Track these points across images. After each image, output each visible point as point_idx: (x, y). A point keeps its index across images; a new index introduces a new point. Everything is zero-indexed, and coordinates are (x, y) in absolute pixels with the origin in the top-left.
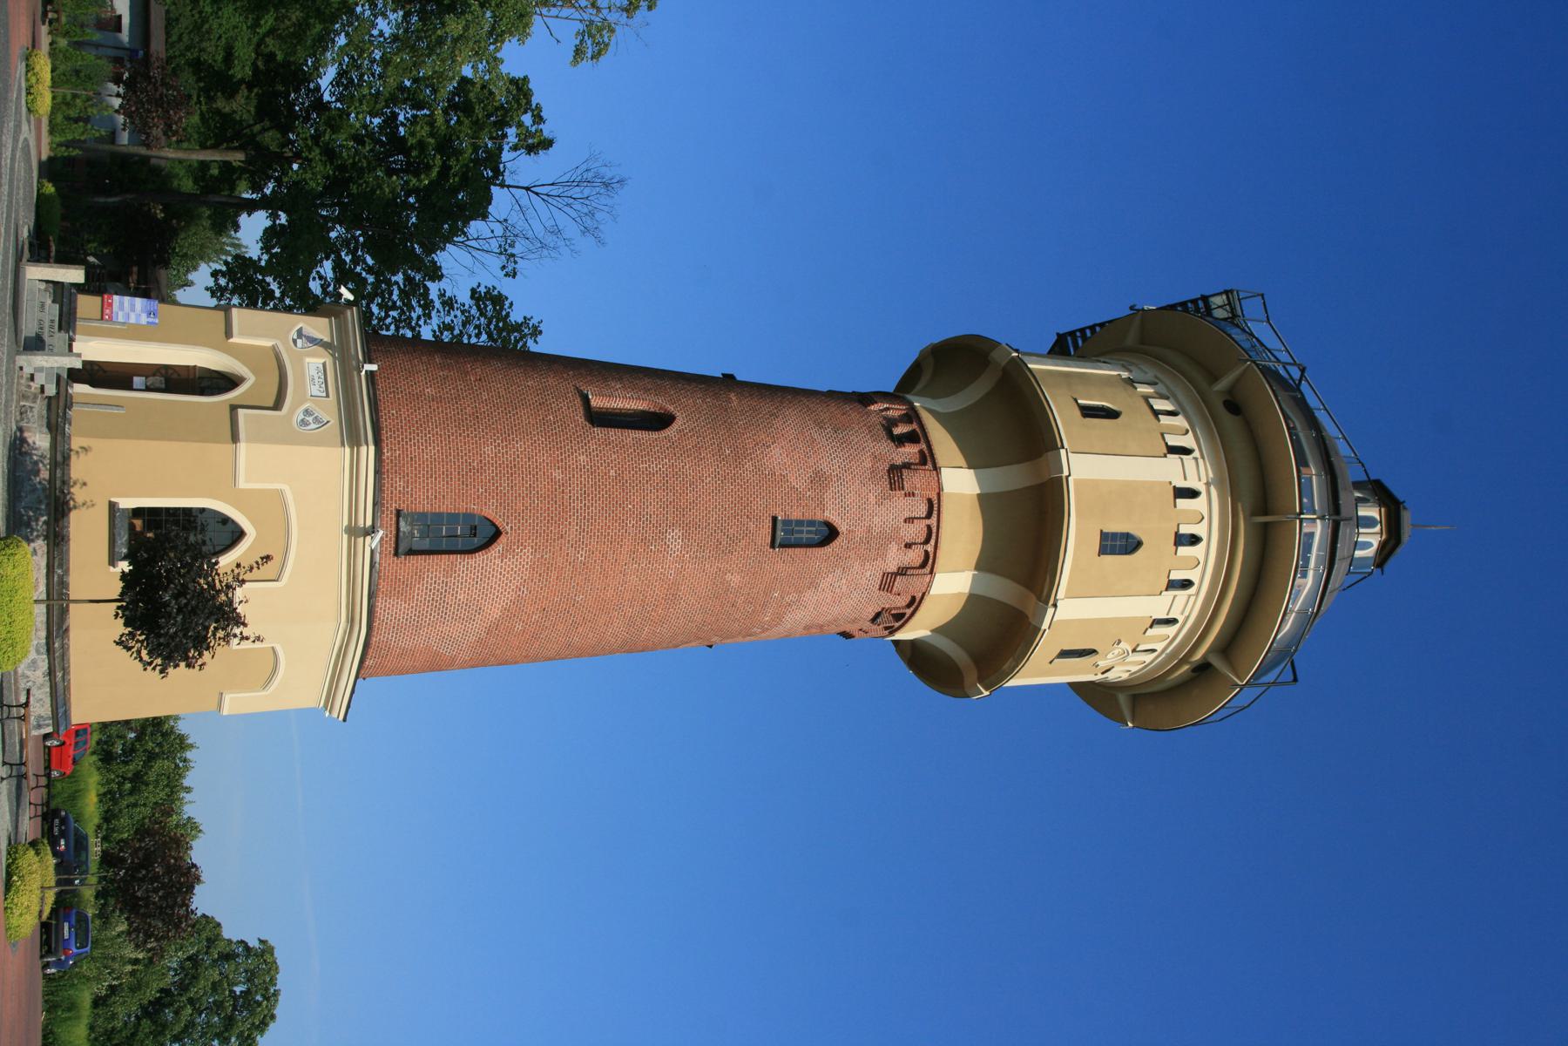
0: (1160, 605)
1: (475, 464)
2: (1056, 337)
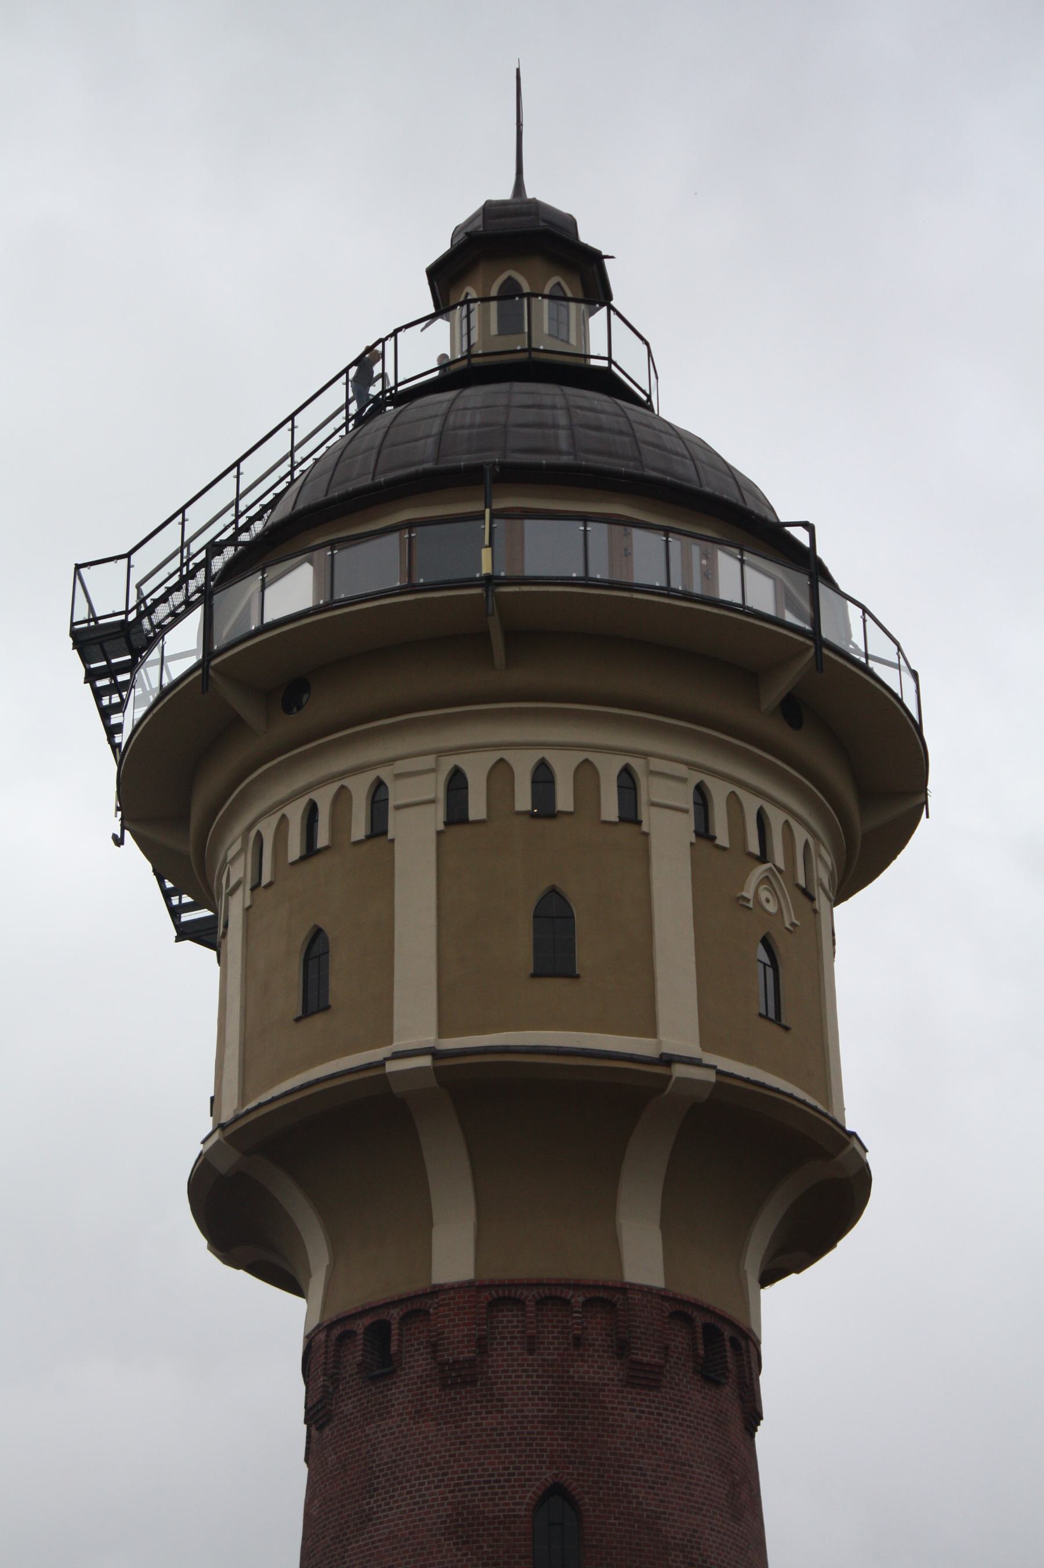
2: (188, 943)
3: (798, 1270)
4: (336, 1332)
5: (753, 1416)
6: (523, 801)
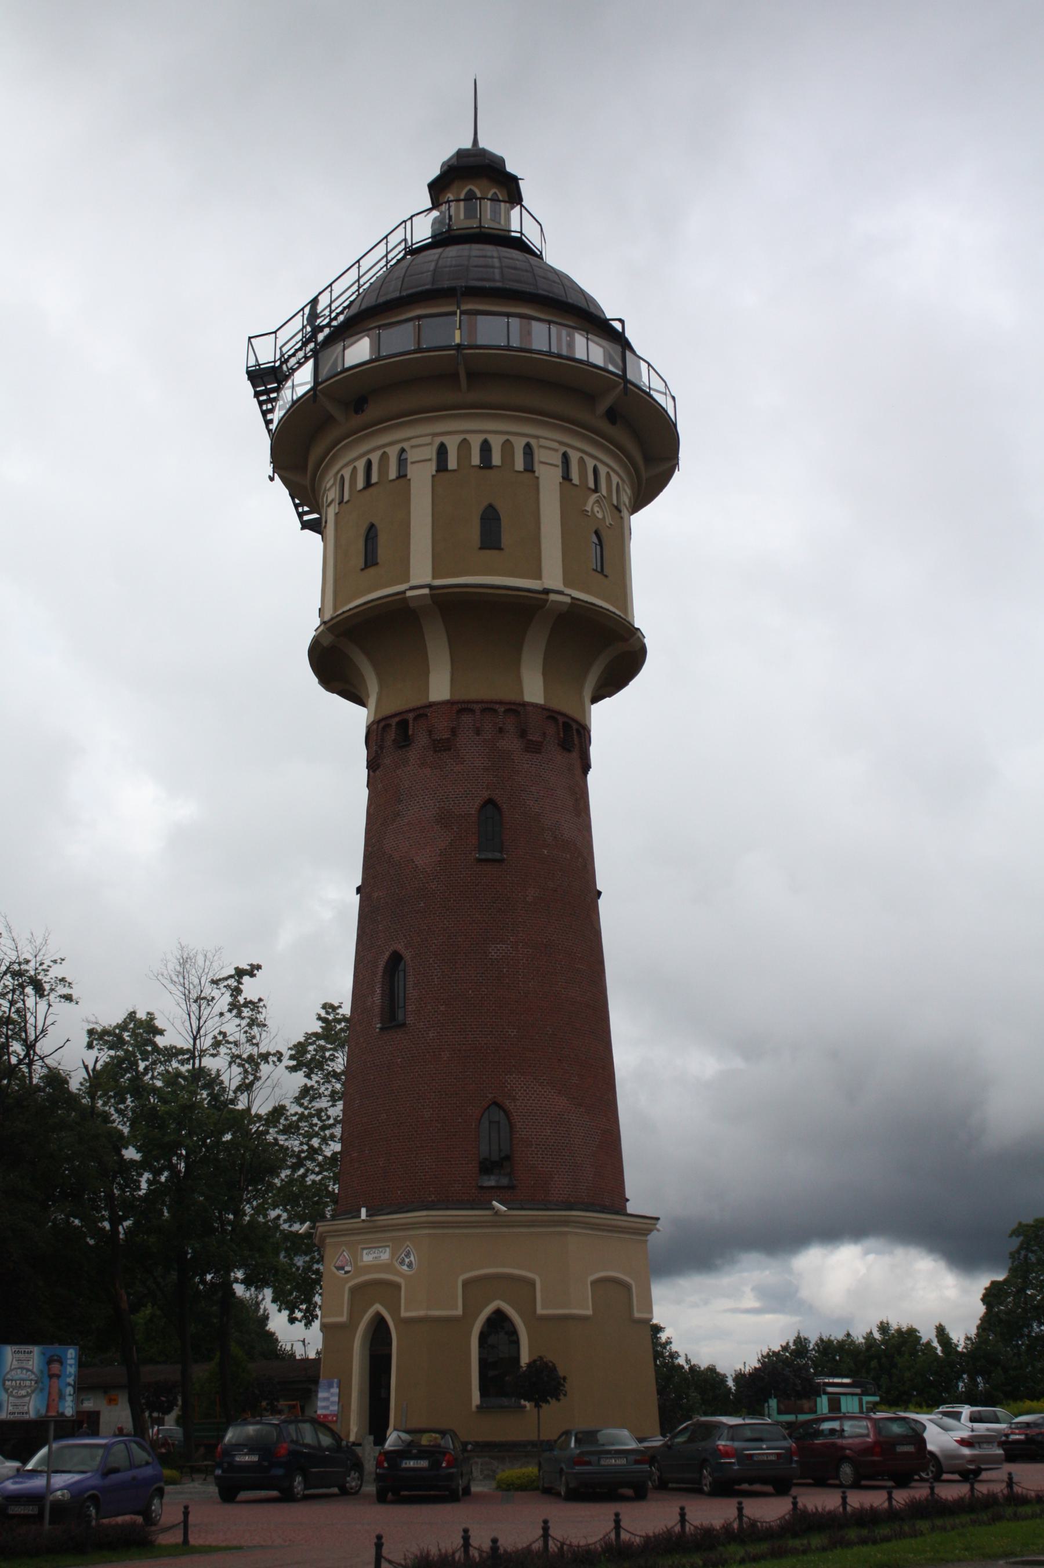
0: (549, 478)
1: (439, 1125)
3: (610, 696)
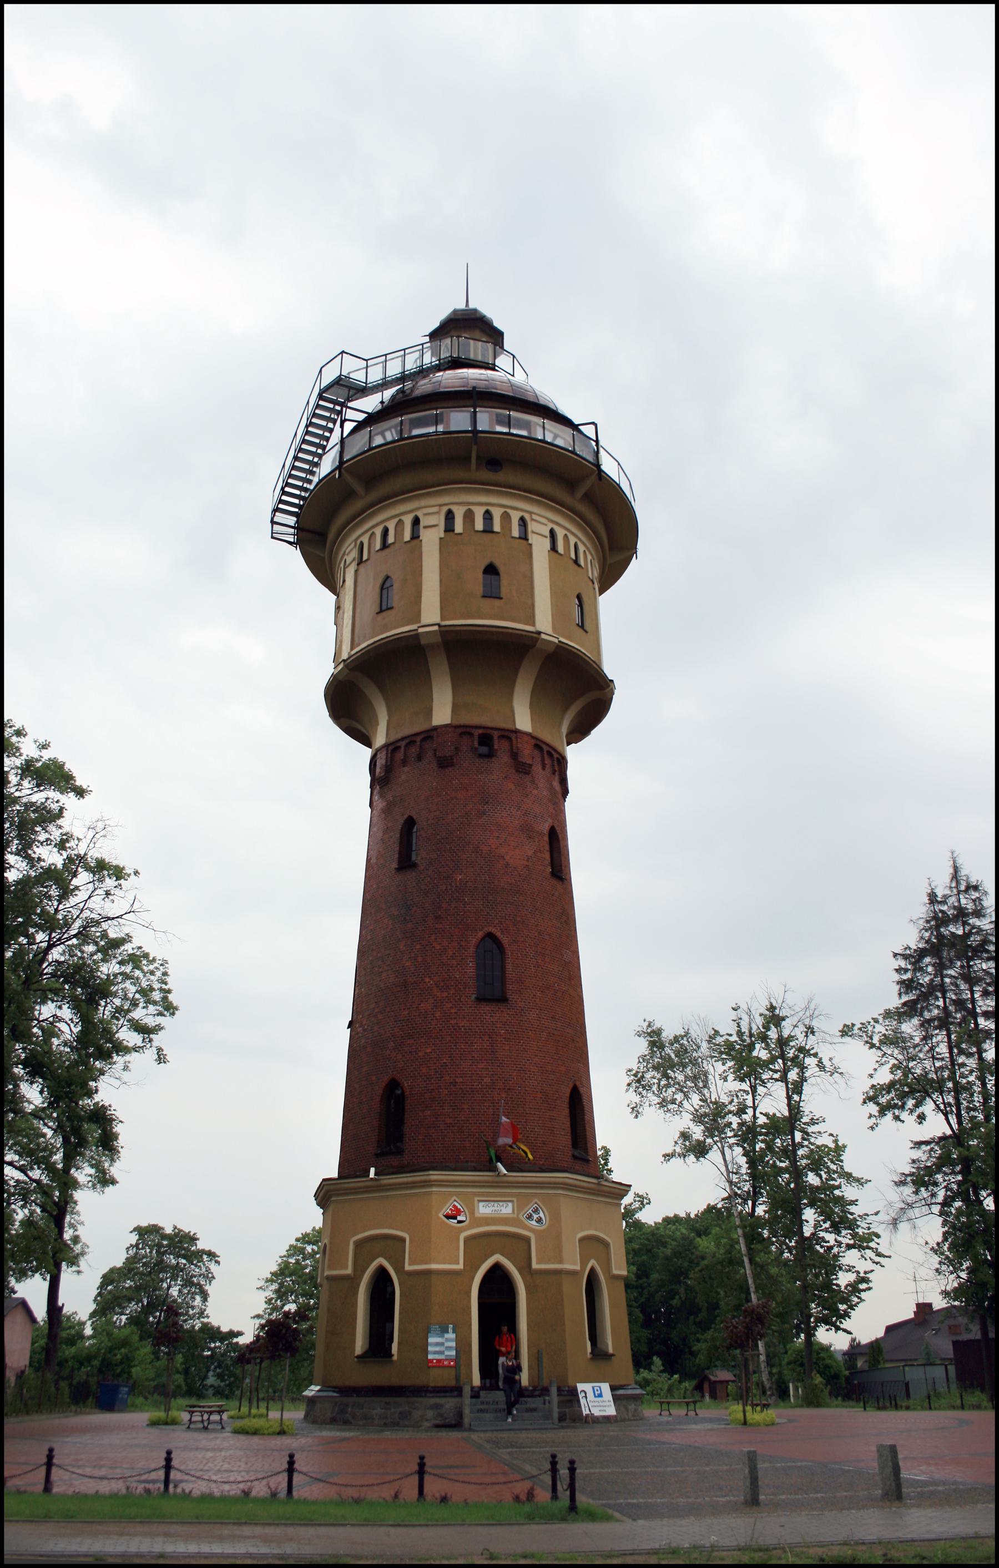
0: (540, 546)
4: (390, 748)
5: (565, 792)
6: (479, 525)
